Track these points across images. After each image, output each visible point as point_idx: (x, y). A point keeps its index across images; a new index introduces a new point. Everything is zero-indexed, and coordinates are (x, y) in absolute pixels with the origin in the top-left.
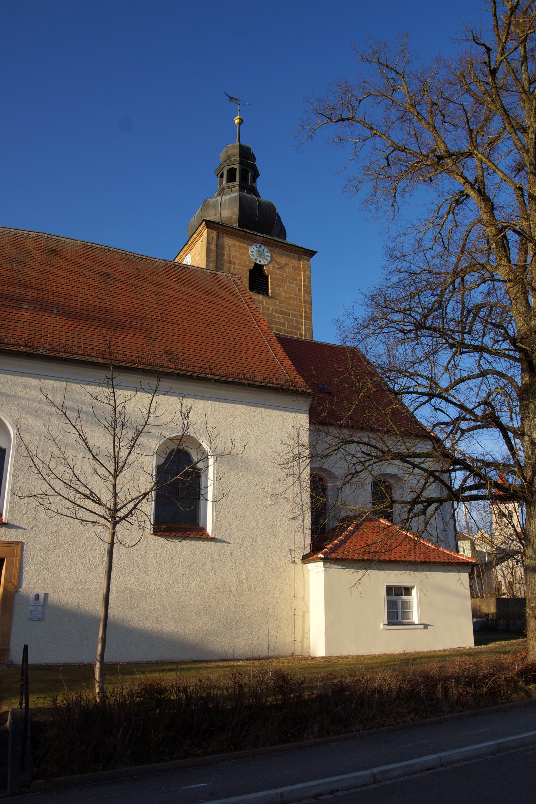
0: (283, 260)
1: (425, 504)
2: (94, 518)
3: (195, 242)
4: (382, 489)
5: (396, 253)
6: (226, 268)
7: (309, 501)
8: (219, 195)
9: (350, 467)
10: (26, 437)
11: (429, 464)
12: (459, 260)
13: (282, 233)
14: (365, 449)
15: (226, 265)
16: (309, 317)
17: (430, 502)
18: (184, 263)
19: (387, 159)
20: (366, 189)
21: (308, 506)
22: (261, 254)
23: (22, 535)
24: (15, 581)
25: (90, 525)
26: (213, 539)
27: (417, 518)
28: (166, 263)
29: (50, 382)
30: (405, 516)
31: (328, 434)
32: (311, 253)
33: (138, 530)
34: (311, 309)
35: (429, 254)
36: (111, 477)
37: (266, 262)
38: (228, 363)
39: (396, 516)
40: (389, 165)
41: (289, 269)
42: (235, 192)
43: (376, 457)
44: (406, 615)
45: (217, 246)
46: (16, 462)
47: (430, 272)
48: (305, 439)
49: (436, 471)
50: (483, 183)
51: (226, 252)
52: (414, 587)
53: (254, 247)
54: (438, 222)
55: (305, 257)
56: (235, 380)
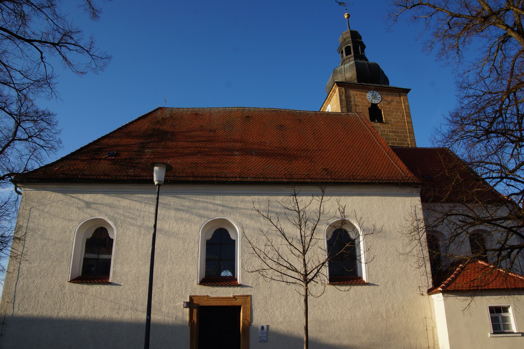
0: (389, 98)
1: (509, 250)
2: (294, 280)
3: (332, 97)
4: (478, 243)
5: (464, 85)
6: (353, 109)
7: (428, 255)
8: (342, 65)
9: (453, 231)
10: (246, 231)
11: (509, 223)
12: (510, 82)
13: (386, 81)
14: (460, 218)
15: (354, 107)
16: (412, 132)
17: (513, 248)
18: (327, 111)
19: (449, 24)
20: (438, 46)
21: (427, 258)
22: (374, 97)
23: (250, 291)
24: (249, 319)
25: (292, 284)
26: (367, 284)
27: (504, 261)
28: (316, 113)
29: (257, 197)
30: (495, 259)
31: (435, 211)
32: (407, 91)
33: (322, 287)
34: (412, 127)
35: (488, 81)
36: (301, 254)
37: (379, 101)
38: (364, 171)
39: (489, 257)
40: (450, 28)
41: (394, 103)
42: (352, 61)
43: (470, 223)
44: (507, 327)
45: (346, 97)
46: (242, 247)
47: (490, 93)
48: (421, 216)
49: (514, 227)
50: (521, 24)
51: (352, 99)
52: (509, 306)
53: (369, 93)
54: (491, 59)
55: (404, 94)
56: (370, 181)
